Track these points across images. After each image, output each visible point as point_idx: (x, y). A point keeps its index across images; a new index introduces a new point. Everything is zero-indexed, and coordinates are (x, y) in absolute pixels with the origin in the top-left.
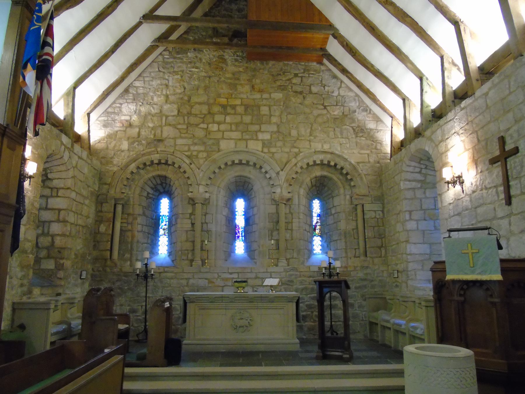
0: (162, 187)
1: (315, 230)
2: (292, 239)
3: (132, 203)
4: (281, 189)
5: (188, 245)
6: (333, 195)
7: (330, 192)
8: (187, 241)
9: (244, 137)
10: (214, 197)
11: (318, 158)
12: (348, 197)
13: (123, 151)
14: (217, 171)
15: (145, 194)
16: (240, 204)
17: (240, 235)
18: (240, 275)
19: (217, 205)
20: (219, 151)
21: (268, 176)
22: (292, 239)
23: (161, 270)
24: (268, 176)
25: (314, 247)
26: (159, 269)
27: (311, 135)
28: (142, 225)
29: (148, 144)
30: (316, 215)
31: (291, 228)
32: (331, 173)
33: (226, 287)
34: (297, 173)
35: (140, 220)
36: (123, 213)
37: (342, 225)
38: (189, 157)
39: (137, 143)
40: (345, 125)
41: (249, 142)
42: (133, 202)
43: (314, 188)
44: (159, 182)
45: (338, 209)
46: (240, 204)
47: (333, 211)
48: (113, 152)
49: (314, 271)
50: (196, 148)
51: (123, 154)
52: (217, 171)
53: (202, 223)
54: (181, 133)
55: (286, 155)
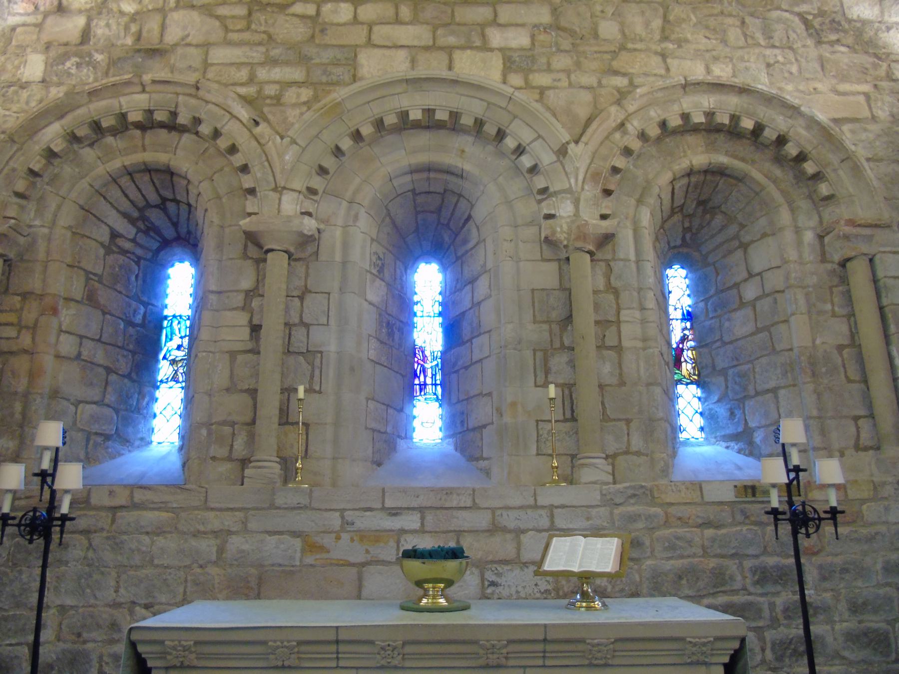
1: (678, 364)
2: (622, 383)
3: (41, 255)
4: (576, 202)
6: (746, 239)
7: (733, 229)
9: (441, 42)
10: (334, 236)
11: (698, 106)
12: (809, 236)
13: (24, 86)
14: (346, 144)
15: (103, 235)
16: (428, 281)
17: (429, 381)
18: (429, 518)
19: (344, 263)
20: (354, 79)
21: (526, 161)
22: (622, 383)
23: (121, 500)
24: (526, 161)
25: (683, 421)
27: (665, 38)
28: (81, 337)
29: (113, 63)
30: (678, 314)
31: (614, 343)
32: (743, 160)
33: (372, 568)
34: (627, 152)
35: (67, 316)
37: (798, 334)
38: (247, 100)
39: (75, 60)
40: (779, 8)
41: (457, 55)
42: (48, 253)
43: (677, 218)
44: (153, 198)
45: (774, 281)
46: (428, 281)
47: (750, 292)
49: (721, 503)
50: (277, 73)
51: (24, 94)
52: (346, 144)
54: (227, 29)
55: (586, 97)
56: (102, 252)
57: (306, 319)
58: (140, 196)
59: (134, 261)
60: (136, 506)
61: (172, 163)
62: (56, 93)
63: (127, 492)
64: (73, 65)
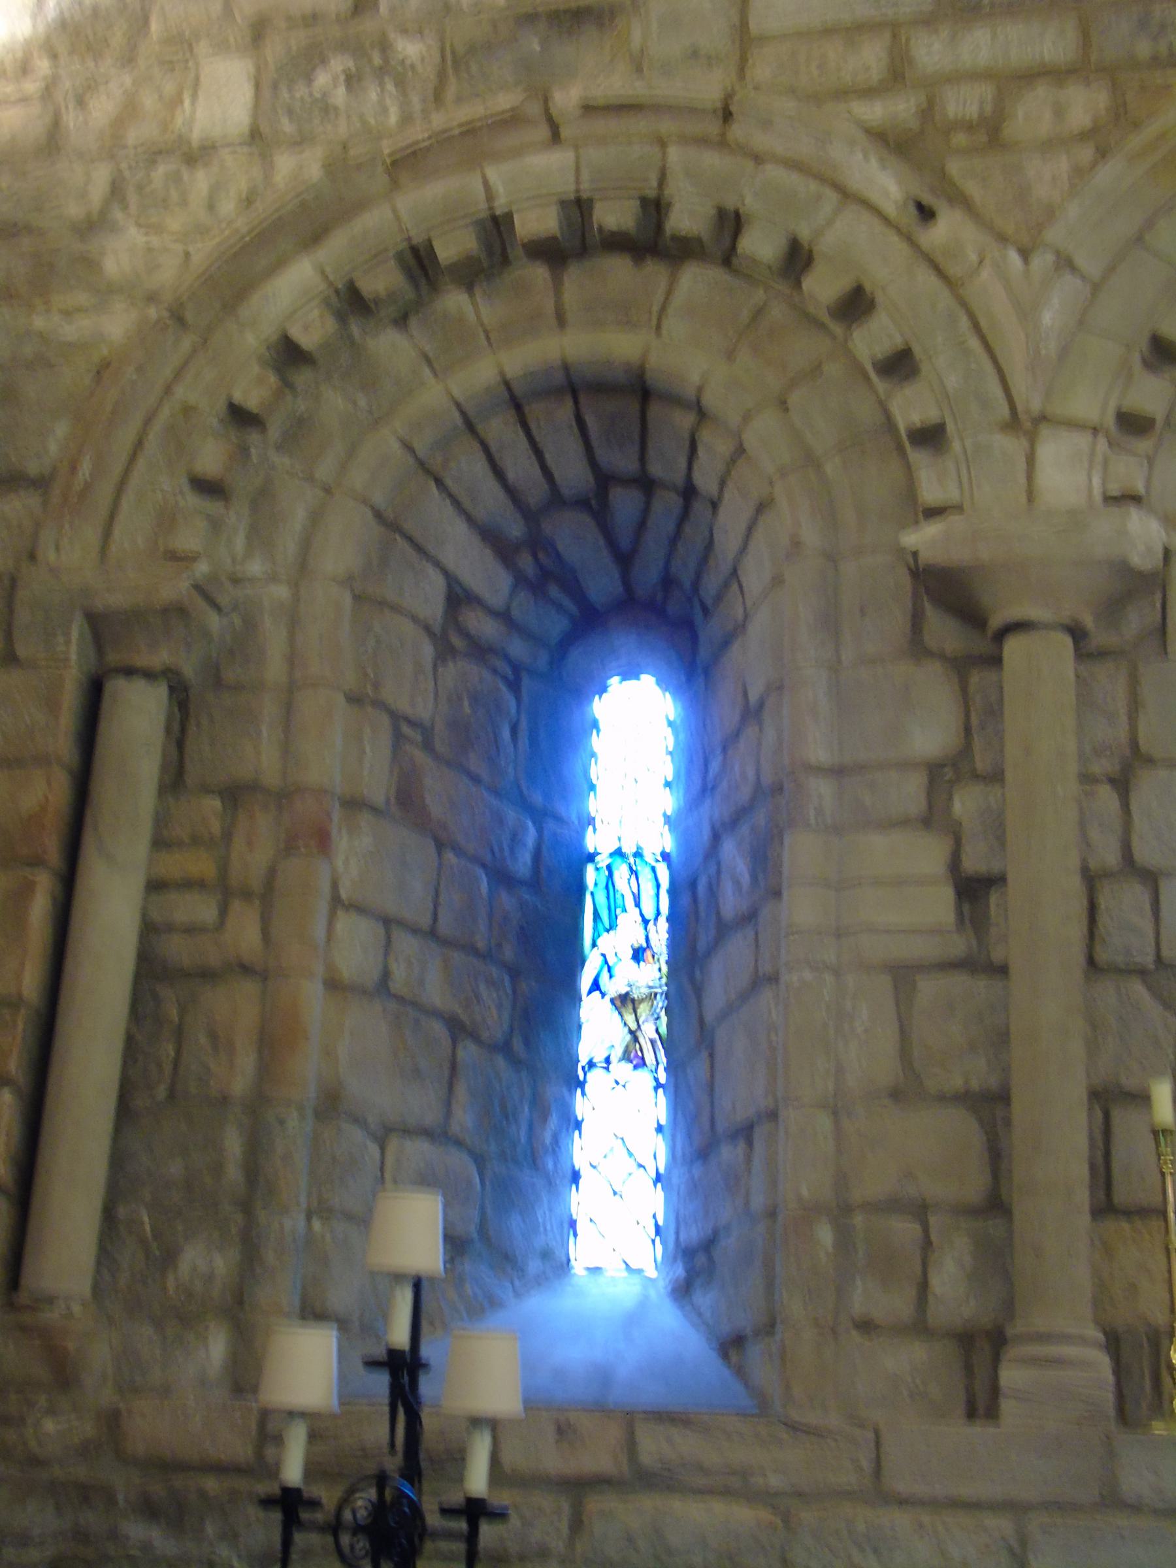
0: (610, 535)
3: (274, 669)
5: (929, 1150)
8: (905, 1092)
13: (195, 155)
23: (598, 1457)
26: (564, 1431)
28: (387, 922)
29: (455, 63)
35: (356, 856)
36: (174, 779)
38: (894, 143)
42: (292, 659)
44: (573, 473)
48: (102, 176)
50: (980, 45)
51: (200, 181)
53: (1091, 880)
56: (428, 650)
57: (1146, 853)
58: (537, 471)
59: (505, 678)
60: (645, 1479)
61: (654, 361)
62: (297, 169)
63: (614, 1433)
64: (335, 79)
